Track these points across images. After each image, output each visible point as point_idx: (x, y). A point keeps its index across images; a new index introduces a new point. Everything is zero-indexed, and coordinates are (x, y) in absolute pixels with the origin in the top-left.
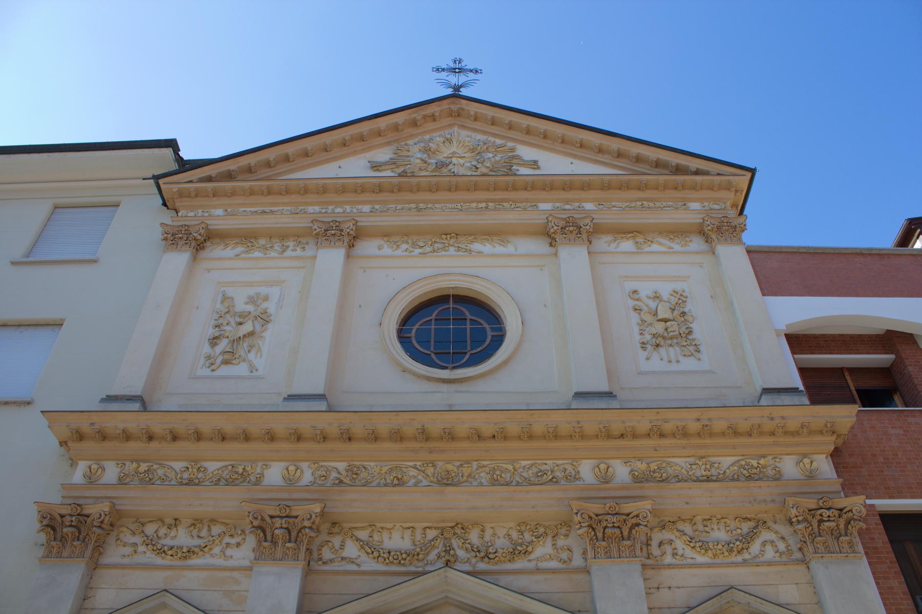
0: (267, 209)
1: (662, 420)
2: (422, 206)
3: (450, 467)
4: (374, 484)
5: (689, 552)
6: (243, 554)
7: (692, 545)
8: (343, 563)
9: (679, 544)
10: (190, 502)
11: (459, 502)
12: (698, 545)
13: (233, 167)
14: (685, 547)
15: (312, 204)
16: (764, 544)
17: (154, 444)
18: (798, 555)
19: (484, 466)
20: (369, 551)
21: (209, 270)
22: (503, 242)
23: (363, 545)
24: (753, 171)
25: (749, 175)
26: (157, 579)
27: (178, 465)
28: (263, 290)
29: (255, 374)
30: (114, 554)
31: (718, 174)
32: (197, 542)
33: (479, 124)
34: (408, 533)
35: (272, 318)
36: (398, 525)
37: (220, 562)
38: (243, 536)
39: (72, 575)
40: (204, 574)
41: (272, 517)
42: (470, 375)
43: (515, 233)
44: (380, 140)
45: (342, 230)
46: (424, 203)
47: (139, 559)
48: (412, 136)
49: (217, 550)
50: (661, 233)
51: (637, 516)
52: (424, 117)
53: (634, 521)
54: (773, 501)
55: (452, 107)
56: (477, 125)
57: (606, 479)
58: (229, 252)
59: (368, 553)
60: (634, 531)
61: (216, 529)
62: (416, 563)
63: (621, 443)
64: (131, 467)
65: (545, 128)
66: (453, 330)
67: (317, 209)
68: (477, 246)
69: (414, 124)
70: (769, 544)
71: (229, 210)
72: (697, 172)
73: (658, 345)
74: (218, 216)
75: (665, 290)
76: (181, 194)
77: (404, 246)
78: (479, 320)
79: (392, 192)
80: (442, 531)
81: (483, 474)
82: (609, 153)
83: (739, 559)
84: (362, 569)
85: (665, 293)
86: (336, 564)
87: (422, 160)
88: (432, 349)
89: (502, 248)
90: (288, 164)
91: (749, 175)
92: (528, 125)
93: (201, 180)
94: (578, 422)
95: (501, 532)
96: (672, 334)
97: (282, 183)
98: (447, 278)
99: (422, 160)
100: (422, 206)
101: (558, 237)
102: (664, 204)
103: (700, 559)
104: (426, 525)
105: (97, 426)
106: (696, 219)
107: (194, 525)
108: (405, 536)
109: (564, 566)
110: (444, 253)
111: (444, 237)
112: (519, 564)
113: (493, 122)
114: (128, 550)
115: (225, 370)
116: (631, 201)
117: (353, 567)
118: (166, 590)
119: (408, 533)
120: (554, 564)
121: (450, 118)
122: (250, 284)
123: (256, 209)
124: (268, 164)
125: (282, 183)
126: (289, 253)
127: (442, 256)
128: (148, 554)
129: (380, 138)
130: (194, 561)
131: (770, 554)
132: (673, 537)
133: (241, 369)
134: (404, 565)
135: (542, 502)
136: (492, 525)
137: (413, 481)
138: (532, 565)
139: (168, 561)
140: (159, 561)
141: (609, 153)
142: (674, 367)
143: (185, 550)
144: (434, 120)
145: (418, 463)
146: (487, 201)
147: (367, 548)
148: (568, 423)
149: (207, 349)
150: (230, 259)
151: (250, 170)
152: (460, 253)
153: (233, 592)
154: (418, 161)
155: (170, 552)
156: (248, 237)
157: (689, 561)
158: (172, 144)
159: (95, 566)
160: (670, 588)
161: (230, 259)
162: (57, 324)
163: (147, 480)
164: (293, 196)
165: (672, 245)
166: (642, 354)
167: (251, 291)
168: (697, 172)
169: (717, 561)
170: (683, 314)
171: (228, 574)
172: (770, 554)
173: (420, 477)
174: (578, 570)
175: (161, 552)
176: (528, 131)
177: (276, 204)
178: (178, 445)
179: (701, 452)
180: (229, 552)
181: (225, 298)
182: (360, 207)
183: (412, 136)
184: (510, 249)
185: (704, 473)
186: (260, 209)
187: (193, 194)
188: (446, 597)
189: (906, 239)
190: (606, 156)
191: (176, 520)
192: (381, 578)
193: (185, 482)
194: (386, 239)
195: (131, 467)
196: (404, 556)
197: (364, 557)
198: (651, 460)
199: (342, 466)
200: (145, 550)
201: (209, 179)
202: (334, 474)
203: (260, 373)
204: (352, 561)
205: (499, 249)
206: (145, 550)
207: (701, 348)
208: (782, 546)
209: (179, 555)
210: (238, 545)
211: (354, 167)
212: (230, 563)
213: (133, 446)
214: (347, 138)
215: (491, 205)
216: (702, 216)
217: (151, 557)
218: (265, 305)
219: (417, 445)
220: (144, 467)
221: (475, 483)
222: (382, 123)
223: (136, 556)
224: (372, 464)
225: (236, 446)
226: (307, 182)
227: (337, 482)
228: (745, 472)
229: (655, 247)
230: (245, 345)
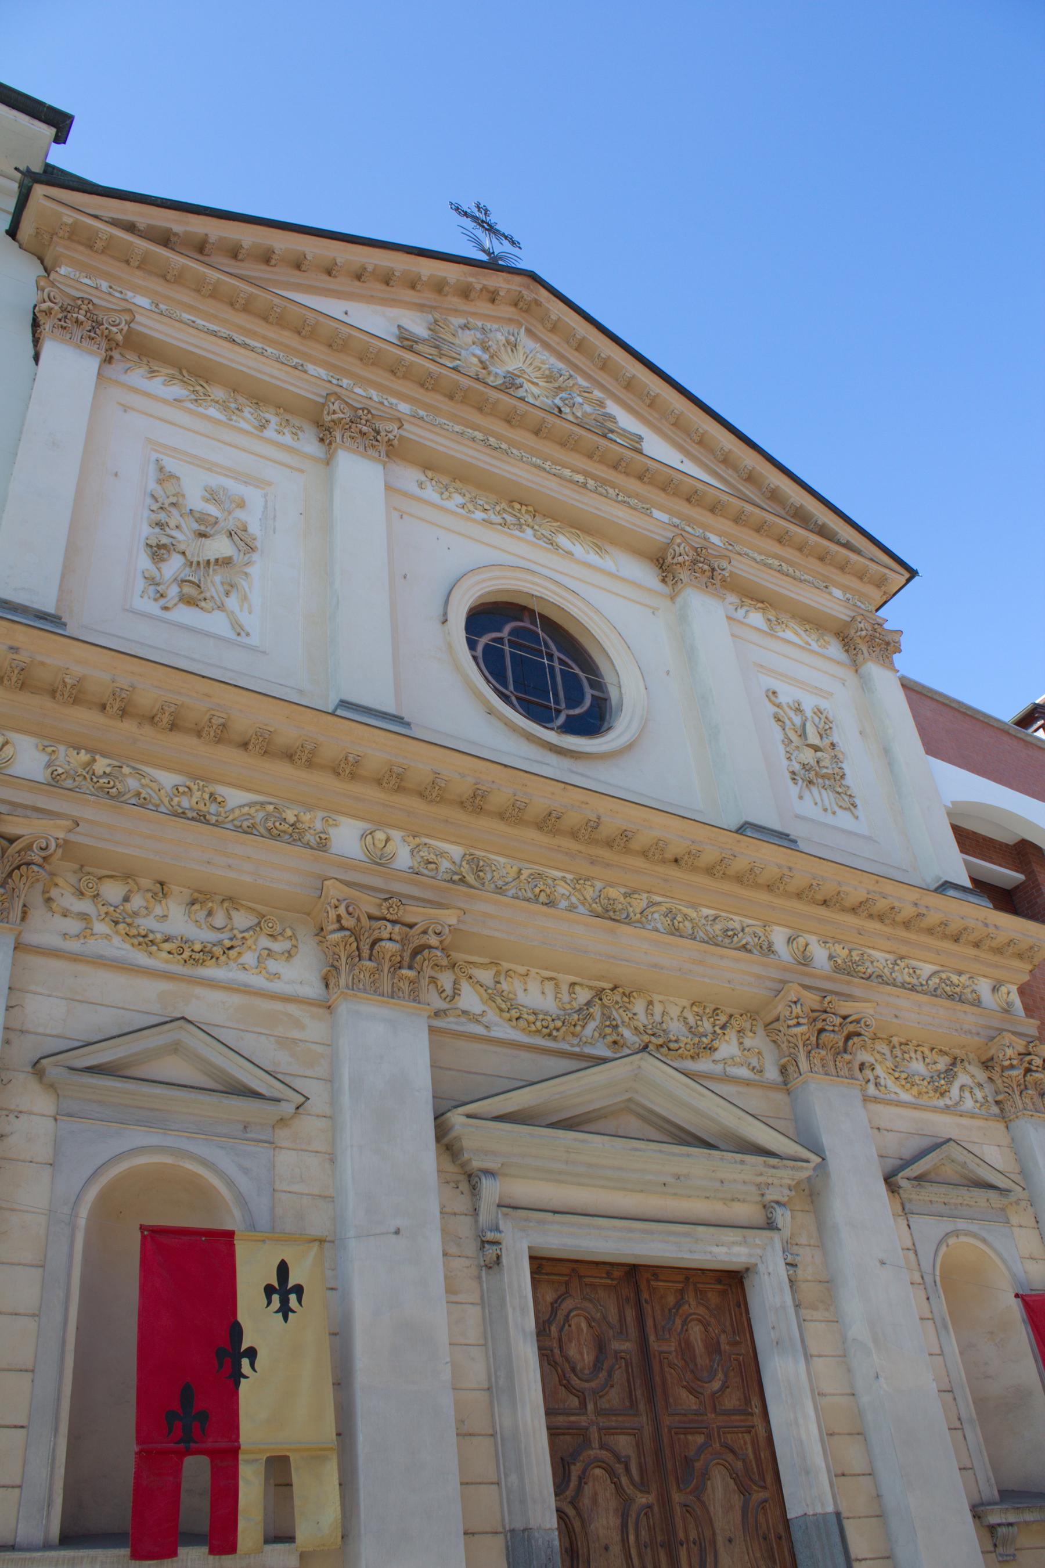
0: (239, 338)
1: (880, 893)
2: (492, 441)
3: (613, 893)
4: (510, 893)
6: (300, 973)
7: (897, 1075)
8: (463, 1020)
10: (198, 854)
11: (637, 951)
12: (904, 1075)
13: (177, 228)
15: (315, 362)
16: (962, 1088)
17: (128, 726)
18: (995, 1110)
19: (659, 904)
20: (503, 1006)
21: (126, 408)
22: (600, 550)
23: (494, 995)
24: (913, 573)
25: (907, 575)
26: (146, 996)
27: (168, 779)
28: (235, 488)
29: (243, 639)
31: (872, 560)
32: (212, 936)
33: (556, 338)
34: (549, 986)
35: (258, 544)
36: (533, 971)
37: (258, 981)
38: (294, 942)
40: (236, 999)
41: (371, 917)
42: (588, 749)
43: (614, 542)
44: (409, 295)
45: (378, 433)
46: (497, 439)
47: (94, 946)
48: (456, 310)
49: (249, 958)
50: (793, 617)
51: (858, 1021)
52: (484, 288)
53: (851, 1028)
54: (978, 1034)
55: (525, 292)
56: (553, 340)
57: (805, 960)
58: (157, 386)
59: (501, 1010)
60: (850, 1042)
61: (242, 920)
62: (570, 1038)
63: (822, 911)
64: (74, 760)
65: (658, 391)
68: (562, 540)
69: (465, 293)
70: (969, 1087)
71: (162, 307)
72: (847, 546)
73: (810, 782)
74: (142, 304)
75: (809, 703)
76: (74, 234)
77: (459, 499)
78: (570, 662)
79: (451, 397)
80: (599, 993)
81: (656, 916)
82: (735, 468)
83: (941, 1103)
84: (493, 1034)
85: (808, 707)
86: (451, 1019)
87: (481, 362)
88: (511, 688)
89: (597, 557)
90: (263, 267)
91: (907, 575)
92: (634, 376)
93: (115, 223)
94: (790, 869)
95: (674, 1012)
96: (825, 770)
97: (277, 301)
98: (529, 577)
99: (481, 362)
100: (492, 441)
101: (684, 575)
102: (806, 577)
103: (905, 1096)
104: (573, 979)
105: (23, 657)
106: (843, 613)
107: (49, 900)
108: (546, 991)
109: (757, 1077)
110: (517, 533)
111: (517, 506)
114: (73, 926)
115: (184, 614)
116: (768, 556)
117: (479, 1030)
118: (183, 1018)
119: (549, 986)
120: (744, 1072)
121: (512, 309)
122: (210, 467)
123: (216, 328)
124: (267, 258)
125: (277, 301)
126: (270, 433)
127: (512, 536)
128: (116, 941)
129: (411, 292)
130: (210, 971)
132: (872, 1060)
133: (216, 623)
134: (555, 1039)
135: (735, 977)
136: (661, 997)
137: (564, 904)
138: (718, 1068)
139: (157, 961)
140: (142, 959)
141: (735, 468)
142: (829, 819)
143: (198, 947)
144: (493, 301)
145: (569, 876)
146: (586, 474)
147: (499, 1000)
148: (780, 867)
149: (144, 562)
150: (165, 401)
151: (201, 248)
152: (541, 542)
153: (294, 1041)
154: (475, 360)
155: (167, 946)
156: (195, 372)
157: (893, 1096)
158: (60, 123)
160: (879, 1129)
161: (165, 401)
163: (109, 793)
164: (286, 333)
165: (809, 640)
166: (794, 790)
167: (215, 481)
168: (847, 546)
169: (921, 1102)
170: (833, 745)
171: (279, 1006)
172: (969, 1104)
173: (574, 900)
174: (771, 1086)
175: (146, 941)
176: (629, 385)
177: (252, 334)
178: (177, 739)
179: (903, 950)
180: (272, 965)
181: (165, 477)
182: (394, 401)
183: (456, 310)
184: (608, 563)
185: (908, 979)
186: (224, 332)
187: (99, 245)
188: (630, 1100)
189: (1026, 720)
190: (730, 472)
191: (162, 884)
192: (524, 1055)
193: (190, 814)
194: (430, 473)
195: (74, 760)
196: (559, 1023)
197: (492, 1016)
198: (855, 946)
199: (456, 851)
200: (108, 931)
201: (131, 228)
202: (445, 865)
203: (254, 640)
204: (476, 1019)
205: (593, 558)
206: (108, 931)
207: (858, 802)
208: (979, 1095)
209: (186, 955)
210: (289, 955)
211: (375, 319)
212: (277, 987)
213: (83, 719)
214: (370, 268)
215: (591, 483)
216: (852, 614)
217: (119, 947)
218: (240, 514)
219: (574, 846)
220: (102, 765)
221: (650, 927)
222: (427, 268)
223: (91, 941)
224: (502, 860)
225: (284, 770)
226: (321, 319)
227: (456, 878)
228: (948, 989)
229: (789, 635)
230: (218, 579)
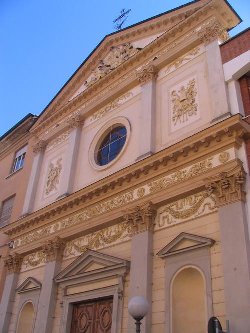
5: (174, 219)
9: (171, 216)
14: (173, 217)
30: (24, 268)
39: (144, 236)
65: (126, 34)
66: (112, 143)
67: (71, 115)
68: (121, 102)
112: (118, 241)
113: (152, 28)
131: (207, 211)
159: (152, 232)
162: (14, 196)
172: (207, 211)
176: (134, 34)
